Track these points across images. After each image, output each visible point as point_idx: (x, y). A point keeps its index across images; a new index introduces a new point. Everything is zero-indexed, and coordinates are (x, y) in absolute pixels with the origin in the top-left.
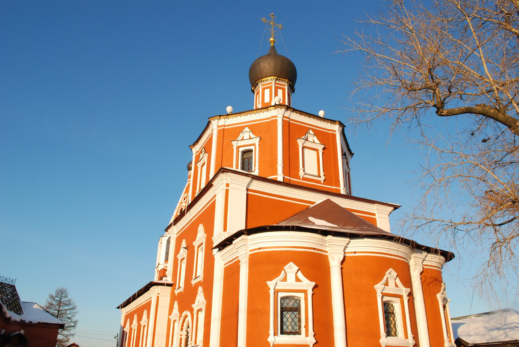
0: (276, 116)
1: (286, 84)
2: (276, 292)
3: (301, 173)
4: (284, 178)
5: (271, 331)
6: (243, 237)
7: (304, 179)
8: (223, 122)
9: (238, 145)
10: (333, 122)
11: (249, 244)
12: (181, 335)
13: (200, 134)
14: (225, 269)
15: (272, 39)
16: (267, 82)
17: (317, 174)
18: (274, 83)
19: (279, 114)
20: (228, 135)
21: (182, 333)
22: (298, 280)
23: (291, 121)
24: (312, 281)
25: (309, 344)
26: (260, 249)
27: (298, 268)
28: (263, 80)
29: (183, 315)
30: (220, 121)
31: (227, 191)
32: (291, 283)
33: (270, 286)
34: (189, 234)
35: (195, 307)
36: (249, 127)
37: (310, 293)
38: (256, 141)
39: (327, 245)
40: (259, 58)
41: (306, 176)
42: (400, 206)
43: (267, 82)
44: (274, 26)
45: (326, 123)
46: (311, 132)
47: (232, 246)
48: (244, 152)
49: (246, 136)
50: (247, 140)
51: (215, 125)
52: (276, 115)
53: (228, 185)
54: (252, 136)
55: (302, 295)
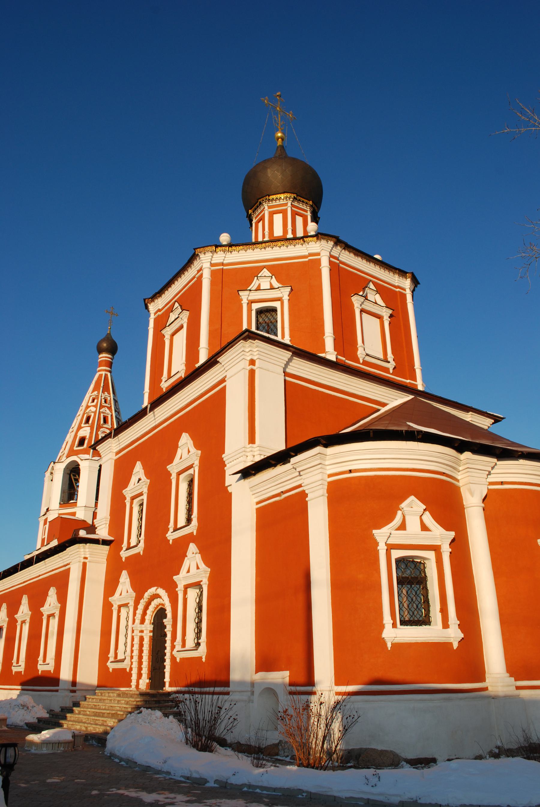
0: (318, 254)
1: (308, 209)
2: (390, 547)
3: (360, 353)
4: (337, 358)
5: (387, 619)
6: (318, 449)
7: (365, 363)
8: (220, 257)
9: (251, 298)
10: (402, 273)
11: (327, 463)
12: (142, 631)
13: (171, 277)
14: (258, 510)
15: (279, 135)
16: (278, 203)
17: (381, 356)
18: (289, 204)
19: (323, 250)
20: (231, 282)
21: (143, 627)
22: (424, 528)
23: (341, 265)
24: (447, 529)
25: (451, 640)
26: (350, 471)
27: (424, 507)
28: (271, 197)
29: (147, 595)
30: (215, 255)
31: (252, 373)
32: (413, 534)
33: (378, 539)
34: (156, 453)
35: (181, 579)
36: (269, 268)
37: (446, 550)
38: (285, 293)
39: (461, 468)
40: (265, 161)
41: (368, 359)
42: (503, 418)
43: (278, 203)
44: (282, 113)
45: (391, 274)
46: (371, 286)
47: (288, 466)
48: (260, 312)
49: (265, 284)
50: (266, 290)
51: (206, 262)
52: (318, 251)
53: (252, 362)
54: (276, 284)
55: (431, 555)
